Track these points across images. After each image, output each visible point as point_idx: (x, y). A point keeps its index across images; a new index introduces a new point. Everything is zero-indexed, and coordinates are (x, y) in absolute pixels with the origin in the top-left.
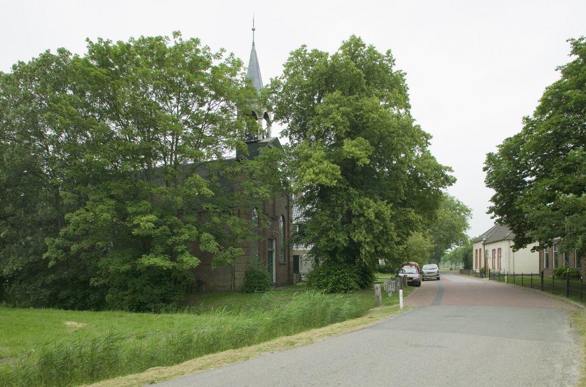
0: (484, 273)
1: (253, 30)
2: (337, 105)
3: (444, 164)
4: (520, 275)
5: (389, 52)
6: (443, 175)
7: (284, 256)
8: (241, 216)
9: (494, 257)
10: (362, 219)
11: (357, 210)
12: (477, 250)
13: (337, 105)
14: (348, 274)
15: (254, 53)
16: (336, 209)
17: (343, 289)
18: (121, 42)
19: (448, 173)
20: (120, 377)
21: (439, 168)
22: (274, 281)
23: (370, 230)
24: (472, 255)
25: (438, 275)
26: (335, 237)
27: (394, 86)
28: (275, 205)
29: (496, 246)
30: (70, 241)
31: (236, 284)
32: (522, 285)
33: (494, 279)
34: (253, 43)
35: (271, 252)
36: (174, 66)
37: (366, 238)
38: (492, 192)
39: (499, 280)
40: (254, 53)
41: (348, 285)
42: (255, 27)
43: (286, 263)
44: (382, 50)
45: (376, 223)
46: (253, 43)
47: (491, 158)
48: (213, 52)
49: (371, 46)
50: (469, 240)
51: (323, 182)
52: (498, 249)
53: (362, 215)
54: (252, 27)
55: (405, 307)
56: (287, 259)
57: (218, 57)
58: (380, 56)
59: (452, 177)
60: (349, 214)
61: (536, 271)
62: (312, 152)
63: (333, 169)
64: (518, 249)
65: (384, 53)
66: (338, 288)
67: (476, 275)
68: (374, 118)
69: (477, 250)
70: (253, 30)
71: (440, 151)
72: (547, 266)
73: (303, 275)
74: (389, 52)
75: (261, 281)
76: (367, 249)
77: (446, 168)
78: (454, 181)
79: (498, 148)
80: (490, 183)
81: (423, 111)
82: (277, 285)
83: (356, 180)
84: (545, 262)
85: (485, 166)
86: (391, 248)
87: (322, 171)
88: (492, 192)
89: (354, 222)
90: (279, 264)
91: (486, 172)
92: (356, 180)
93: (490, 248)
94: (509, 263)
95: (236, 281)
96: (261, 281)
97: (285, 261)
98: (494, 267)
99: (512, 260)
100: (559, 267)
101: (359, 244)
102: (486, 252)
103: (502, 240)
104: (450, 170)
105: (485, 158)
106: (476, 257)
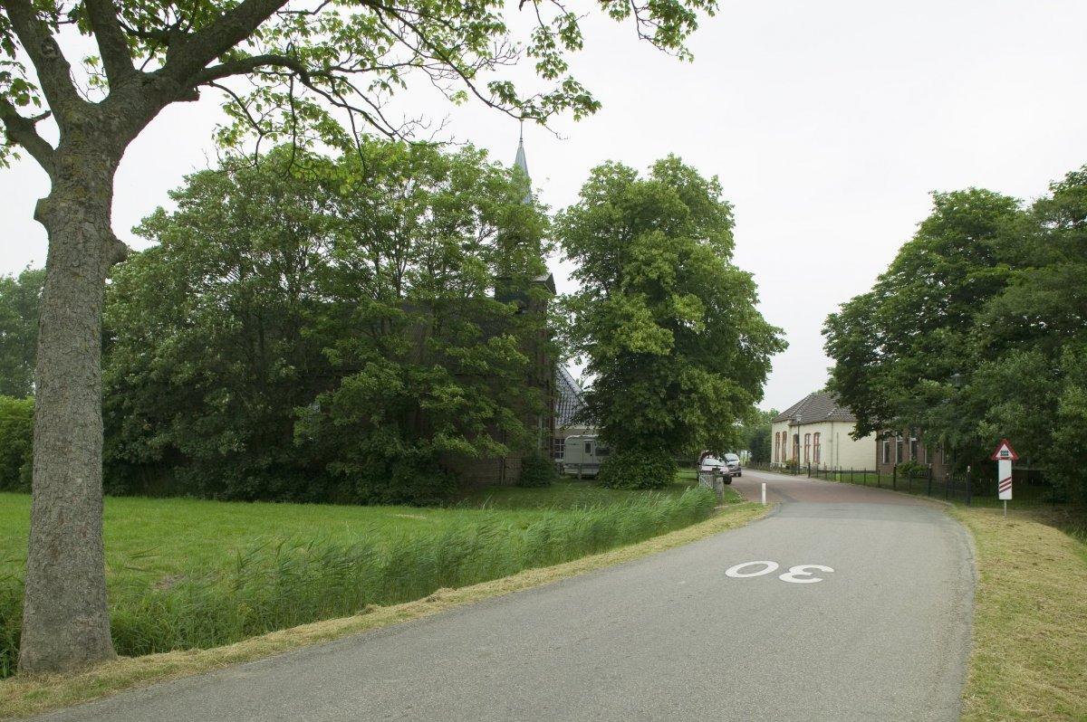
0: (793, 468)
3: (774, 324)
4: (862, 472)
5: (716, 179)
6: (772, 338)
9: (778, 443)
10: (693, 395)
12: (778, 434)
15: (521, 151)
16: (657, 382)
18: (781, 350)
19: (778, 336)
20: (674, 532)
21: (768, 330)
24: (770, 441)
25: (739, 469)
27: (716, 220)
29: (812, 429)
31: (506, 476)
32: (879, 486)
33: (817, 477)
37: (699, 420)
38: (833, 363)
39: (826, 479)
40: (521, 151)
44: (705, 174)
47: (832, 320)
50: (16, 281)
52: (815, 434)
53: (695, 390)
55: (768, 504)
58: (703, 182)
59: (783, 340)
60: (674, 389)
61: (872, 466)
62: (634, 310)
63: (664, 334)
64: (860, 437)
65: (709, 180)
67: (777, 469)
68: (705, 270)
69: (778, 434)
71: (769, 308)
72: (887, 460)
73: (567, 465)
74: (716, 179)
77: (776, 330)
78: (786, 345)
79: (841, 307)
80: (830, 352)
81: (747, 253)
84: (883, 454)
85: (826, 327)
86: (725, 433)
87: (650, 336)
88: (833, 363)
89: (682, 398)
91: (826, 336)
93: (803, 431)
94: (832, 454)
96: (545, 472)
98: (807, 460)
99: (835, 451)
100: (905, 462)
101: (691, 428)
102: (797, 438)
103: (822, 422)
104: (782, 331)
105: (825, 318)
106: (778, 443)
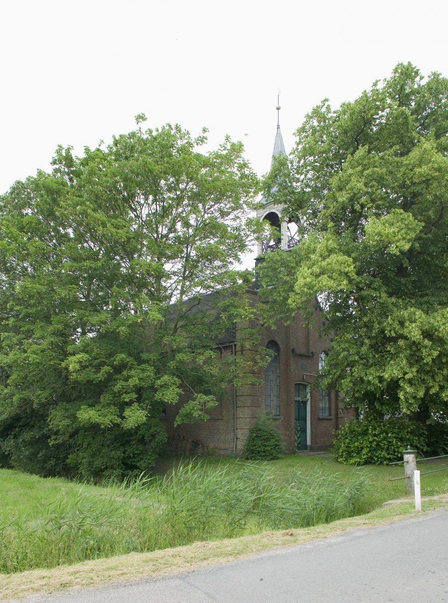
1: (278, 109)
2: (359, 168)
7: (330, 408)
8: (244, 353)
10: (401, 343)
11: (395, 328)
13: (359, 168)
14: (394, 435)
17: (386, 459)
22: (309, 443)
23: (415, 358)
26: (363, 374)
28: (308, 337)
30: (206, 395)
34: (278, 125)
35: (305, 403)
36: (150, 165)
41: (395, 451)
42: (280, 105)
43: (333, 417)
45: (426, 347)
46: (278, 125)
48: (194, 136)
49: (434, 74)
51: (325, 286)
54: (277, 105)
56: (333, 412)
57: (202, 141)
66: (377, 457)
70: (278, 109)
75: (267, 444)
76: (408, 390)
82: (312, 449)
83: (405, 285)
90: (317, 420)
92: (405, 285)
95: (238, 443)
96: (267, 444)
97: (330, 415)
